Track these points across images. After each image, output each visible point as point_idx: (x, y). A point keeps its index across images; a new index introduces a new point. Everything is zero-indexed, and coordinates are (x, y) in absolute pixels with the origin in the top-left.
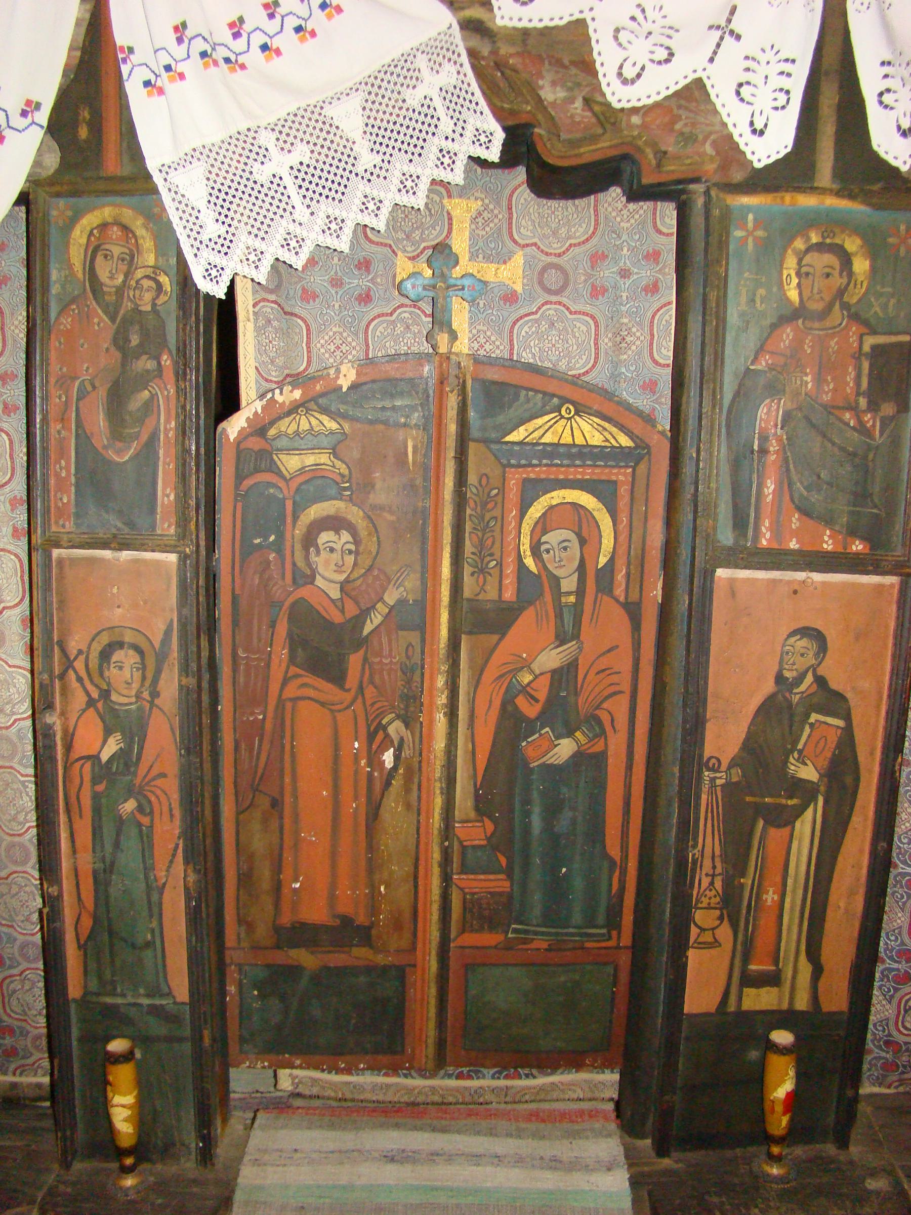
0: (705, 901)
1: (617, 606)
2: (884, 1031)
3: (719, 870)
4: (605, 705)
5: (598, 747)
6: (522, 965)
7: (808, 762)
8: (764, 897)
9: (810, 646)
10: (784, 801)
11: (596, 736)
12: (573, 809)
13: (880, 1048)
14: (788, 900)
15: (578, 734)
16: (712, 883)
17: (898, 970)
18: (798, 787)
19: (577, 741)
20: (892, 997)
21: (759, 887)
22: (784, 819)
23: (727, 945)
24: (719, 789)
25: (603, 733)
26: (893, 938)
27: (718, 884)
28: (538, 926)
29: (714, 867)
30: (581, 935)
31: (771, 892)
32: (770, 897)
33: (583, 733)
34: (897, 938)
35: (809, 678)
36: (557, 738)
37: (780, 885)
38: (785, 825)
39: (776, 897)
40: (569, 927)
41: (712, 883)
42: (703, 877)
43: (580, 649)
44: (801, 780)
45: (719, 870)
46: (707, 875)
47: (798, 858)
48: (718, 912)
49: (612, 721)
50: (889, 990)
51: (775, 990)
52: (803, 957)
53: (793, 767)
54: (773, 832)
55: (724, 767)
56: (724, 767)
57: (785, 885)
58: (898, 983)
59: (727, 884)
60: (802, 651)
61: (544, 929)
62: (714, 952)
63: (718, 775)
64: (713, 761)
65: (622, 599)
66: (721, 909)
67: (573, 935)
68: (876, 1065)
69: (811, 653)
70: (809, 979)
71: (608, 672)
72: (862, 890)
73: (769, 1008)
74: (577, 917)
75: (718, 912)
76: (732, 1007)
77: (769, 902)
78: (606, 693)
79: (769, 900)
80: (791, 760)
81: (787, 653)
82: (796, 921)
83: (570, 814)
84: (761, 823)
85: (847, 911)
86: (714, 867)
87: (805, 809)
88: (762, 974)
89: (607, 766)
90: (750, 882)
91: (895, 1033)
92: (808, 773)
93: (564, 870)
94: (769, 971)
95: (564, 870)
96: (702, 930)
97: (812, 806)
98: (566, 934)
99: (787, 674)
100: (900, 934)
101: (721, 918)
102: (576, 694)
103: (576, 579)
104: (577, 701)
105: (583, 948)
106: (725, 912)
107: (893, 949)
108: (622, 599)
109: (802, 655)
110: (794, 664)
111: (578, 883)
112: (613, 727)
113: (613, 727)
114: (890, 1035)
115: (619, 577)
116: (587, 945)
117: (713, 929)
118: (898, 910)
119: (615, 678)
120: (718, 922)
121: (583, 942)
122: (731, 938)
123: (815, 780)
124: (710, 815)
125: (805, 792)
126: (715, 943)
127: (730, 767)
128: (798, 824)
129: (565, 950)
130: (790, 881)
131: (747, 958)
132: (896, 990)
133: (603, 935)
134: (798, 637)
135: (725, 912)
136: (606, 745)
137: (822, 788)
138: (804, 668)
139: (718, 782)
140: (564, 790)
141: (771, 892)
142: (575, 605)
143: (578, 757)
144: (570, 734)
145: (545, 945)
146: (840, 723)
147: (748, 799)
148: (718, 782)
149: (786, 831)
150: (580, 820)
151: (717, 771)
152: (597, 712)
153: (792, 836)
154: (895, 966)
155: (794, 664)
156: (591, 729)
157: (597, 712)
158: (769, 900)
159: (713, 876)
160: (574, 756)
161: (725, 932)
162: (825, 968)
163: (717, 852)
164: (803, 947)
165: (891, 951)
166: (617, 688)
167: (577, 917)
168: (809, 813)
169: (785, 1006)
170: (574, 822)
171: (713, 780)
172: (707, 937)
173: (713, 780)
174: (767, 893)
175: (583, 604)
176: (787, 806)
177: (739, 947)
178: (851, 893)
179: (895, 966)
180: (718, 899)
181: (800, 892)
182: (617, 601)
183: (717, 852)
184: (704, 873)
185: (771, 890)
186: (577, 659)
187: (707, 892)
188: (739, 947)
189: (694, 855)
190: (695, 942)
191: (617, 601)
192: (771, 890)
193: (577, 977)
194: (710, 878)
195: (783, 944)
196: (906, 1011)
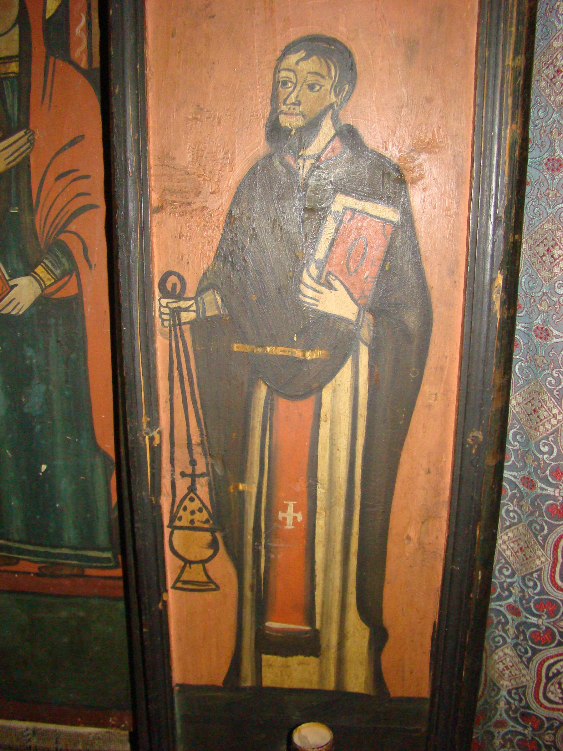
0: (185, 519)
1: (76, 74)
2: (520, 700)
3: (201, 467)
4: (73, 227)
5: (70, 290)
6: (9, 592)
7: (336, 284)
8: (281, 515)
9: (324, 72)
10: (298, 353)
11: (64, 274)
12: (46, 381)
13: (515, 719)
14: (320, 522)
15: (40, 270)
16: (192, 489)
17: (537, 626)
18: (323, 327)
19: (39, 280)
20: (530, 660)
21: (269, 496)
22: (304, 384)
23: (230, 587)
24: (186, 328)
25: (74, 270)
26: (531, 584)
27: (203, 490)
28: (19, 542)
29: (193, 463)
30: (77, 557)
31: (290, 509)
32: (290, 516)
33: (46, 268)
34: (535, 585)
35: (327, 129)
36: (12, 277)
37: (304, 499)
38: (304, 396)
39: (300, 517)
40: (62, 547)
41: (192, 489)
42: (178, 476)
43: (31, 142)
44: (327, 316)
45: (201, 467)
46: (183, 474)
47: (332, 454)
48: (208, 536)
49: (85, 250)
50: (527, 652)
51: (312, 660)
52: (353, 615)
53: (310, 293)
54: (283, 405)
55: (191, 291)
56: (191, 291)
57: (313, 497)
58: (539, 644)
59: (216, 488)
60: (311, 79)
61: (30, 548)
62: (210, 596)
63: (183, 304)
64: (173, 279)
65: (84, 64)
66: (212, 531)
67: (68, 557)
68: (511, 741)
69: (327, 84)
70: (365, 650)
71: (71, 176)
72: (444, 513)
73: (306, 686)
74: (70, 534)
75: (208, 536)
76: (248, 682)
77: (289, 525)
78: (73, 207)
79: (289, 521)
80: (306, 278)
81: (285, 83)
82: (338, 557)
83: (43, 388)
84: (262, 392)
85: (421, 544)
86: (193, 463)
87: (338, 369)
88: (288, 636)
89: (83, 317)
90: (254, 490)
91: (534, 705)
92: (338, 304)
93: (44, 467)
94: (301, 632)
95: (44, 467)
96: (188, 562)
97: (349, 362)
98: (59, 556)
99: (285, 121)
100: (539, 578)
101: (214, 545)
102: (32, 211)
103: (16, 37)
104: (33, 221)
105: (83, 576)
106: (219, 536)
107: (531, 598)
108: (84, 64)
109: (311, 87)
110: (298, 103)
111: (65, 486)
112: (88, 261)
113: (88, 261)
114: (528, 707)
115: (78, 31)
116: (88, 572)
117: (203, 562)
118: (537, 547)
119: (82, 186)
120: (210, 552)
121: (82, 568)
122: (235, 580)
123: (353, 318)
124: (176, 374)
125: (338, 342)
126: (208, 585)
127: (200, 292)
128: (326, 394)
129: (61, 576)
130: (321, 492)
131: (262, 610)
132: (535, 652)
133: (108, 560)
134: (302, 54)
135: (219, 536)
136: (80, 285)
137: (366, 333)
138: (319, 109)
139: (186, 317)
140: (29, 352)
141: (290, 509)
142: (18, 76)
143: (43, 303)
144: (29, 270)
145: (33, 568)
146: (393, 215)
147: (236, 347)
148: (186, 317)
149: (305, 406)
150: (56, 395)
151: (180, 297)
152: (62, 237)
153: (317, 417)
154: (534, 620)
155: (298, 103)
156: (58, 263)
157: (62, 237)
158: (289, 521)
159: (193, 476)
160: (38, 302)
161: (222, 567)
162: (391, 632)
163: (196, 439)
164: (352, 599)
165: (528, 602)
166: (82, 202)
167: (70, 534)
168: (345, 375)
169: (330, 685)
170: (48, 400)
171: (175, 313)
172: (195, 573)
173: (175, 313)
174: (285, 509)
175: (29, 74)
176: (303, 362)
177: (248, 594)
178: (428, 517)
179: (534, 620)
180: (205, 515)
181: (340, 511)
182: (78, 67)
183: (196, 439)
184: (178, 470)
185: (291, 505)
186: (28, 158)
187: (187, 502)
188: (248, 594)
189: (152, 439)
190: (178, 580)
191: (78, 67)
192: (291, 505)
193: (82, 614)
194: (188, 481)
195: (318, 593)
196: (548, 679)
